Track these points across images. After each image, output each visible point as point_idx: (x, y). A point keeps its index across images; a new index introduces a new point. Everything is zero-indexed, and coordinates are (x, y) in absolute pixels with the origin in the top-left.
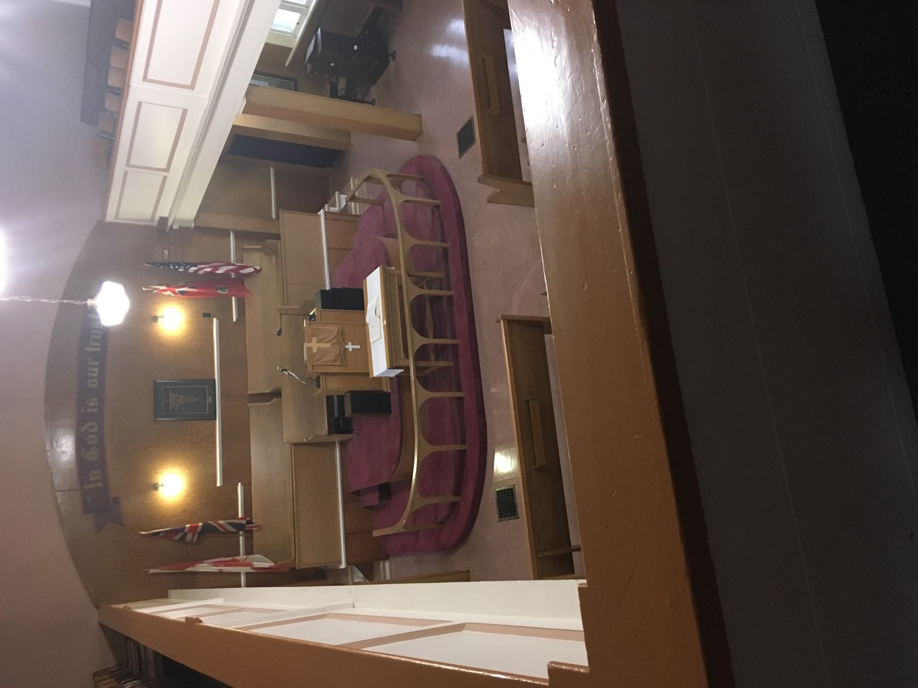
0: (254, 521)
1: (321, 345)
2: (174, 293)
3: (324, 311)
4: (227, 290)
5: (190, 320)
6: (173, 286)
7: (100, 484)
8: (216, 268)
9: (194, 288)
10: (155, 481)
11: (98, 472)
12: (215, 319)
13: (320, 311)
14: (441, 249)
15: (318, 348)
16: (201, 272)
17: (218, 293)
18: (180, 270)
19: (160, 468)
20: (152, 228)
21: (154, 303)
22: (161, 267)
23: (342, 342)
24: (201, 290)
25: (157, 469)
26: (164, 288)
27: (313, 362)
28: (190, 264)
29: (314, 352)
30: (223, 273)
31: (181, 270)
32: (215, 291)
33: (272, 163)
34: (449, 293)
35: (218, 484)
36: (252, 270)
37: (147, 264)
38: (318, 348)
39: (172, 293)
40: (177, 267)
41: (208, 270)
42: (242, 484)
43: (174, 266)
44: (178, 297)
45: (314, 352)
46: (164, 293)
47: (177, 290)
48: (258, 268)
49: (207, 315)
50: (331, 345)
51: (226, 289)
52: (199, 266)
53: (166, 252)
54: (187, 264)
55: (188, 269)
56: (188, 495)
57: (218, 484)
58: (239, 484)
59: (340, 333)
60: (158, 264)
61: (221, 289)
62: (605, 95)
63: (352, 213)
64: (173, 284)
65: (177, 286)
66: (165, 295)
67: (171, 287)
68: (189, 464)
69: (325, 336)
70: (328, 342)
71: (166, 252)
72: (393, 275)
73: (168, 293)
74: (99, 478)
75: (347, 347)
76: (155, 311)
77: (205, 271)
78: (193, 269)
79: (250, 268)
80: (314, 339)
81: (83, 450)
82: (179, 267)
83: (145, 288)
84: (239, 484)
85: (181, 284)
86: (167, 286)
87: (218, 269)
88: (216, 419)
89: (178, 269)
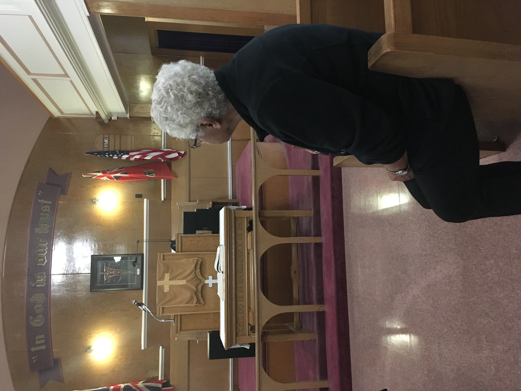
0: (171, 383)
1: (174, 283)
2: (110, 178)
3: (186, 237)
4: (154, 174)
5: (123, 201)
6: (108, 172)
7: (43, 347)
8: (145, 155)
9: (126, 173)
10: (89, 345)
11: (43, 336)
12: (145, 200)
13: (181, 237)
14: (310, 178)
15: (171, 287)
16: (132, 159)
17: (147, 177)
18: (114, 157)
19: (94, 333)
20: (91, 119)
21: (94, 187)
22: (99, 156)
23: (200, 277)
24: (131, 175)
25: (91, 334)
26: (100, 174)
27: (165, 304)
28: (123, 152)
29: (165, 291)
30: (150, 159)
31: (115, 157)
32: (144, 175)
33: (201, 52)
34: (318, 240)
35: (143, 348)
36: (176, 155)
37: (86, 153)
38: (171, 287)
39: (109, 178)
40: (111, 156)
41: (138, 157)
42: (163, 347)
43: (109, 155)
44: (115, 181)
45: (165, 291)
46: (102, 178)
47: (112, 176)
48: (183, 152)
49: (139, 196)
50: (187, 282)
51: (153, 173)
52: (131, 154)
53: (106, 141)
54: (120, 152)
55: (121, 157)
56: (117, 357)
57: (143, 348)
58: (161, 347)
59: (198, 267)
60: (96, 154)
61: (149, 174)
62: (254, 130)
63: (60, 201)
64: (108, 171)
65: (112, 171)
66: (103, 180)
67: (106, 173)
68: (118, 329)
69: (180, 271)
70: (182, 279)
71: (106, 141)
72: (242, 218)
73: (105, 178)
74: (43, 341)
75: (206, 282)
76: (95, 194)
77: (135, 158)
78: (125, 157)
79: (175, 153)
80: (167, 276)
81: (31, 317)
82: (113, 155)
83: (84, 175)
84: (161, 347)
85: (116, 170)
86: (103, 172)
87: (146, 156)
88: (142, 289)
89: (112, 157)
